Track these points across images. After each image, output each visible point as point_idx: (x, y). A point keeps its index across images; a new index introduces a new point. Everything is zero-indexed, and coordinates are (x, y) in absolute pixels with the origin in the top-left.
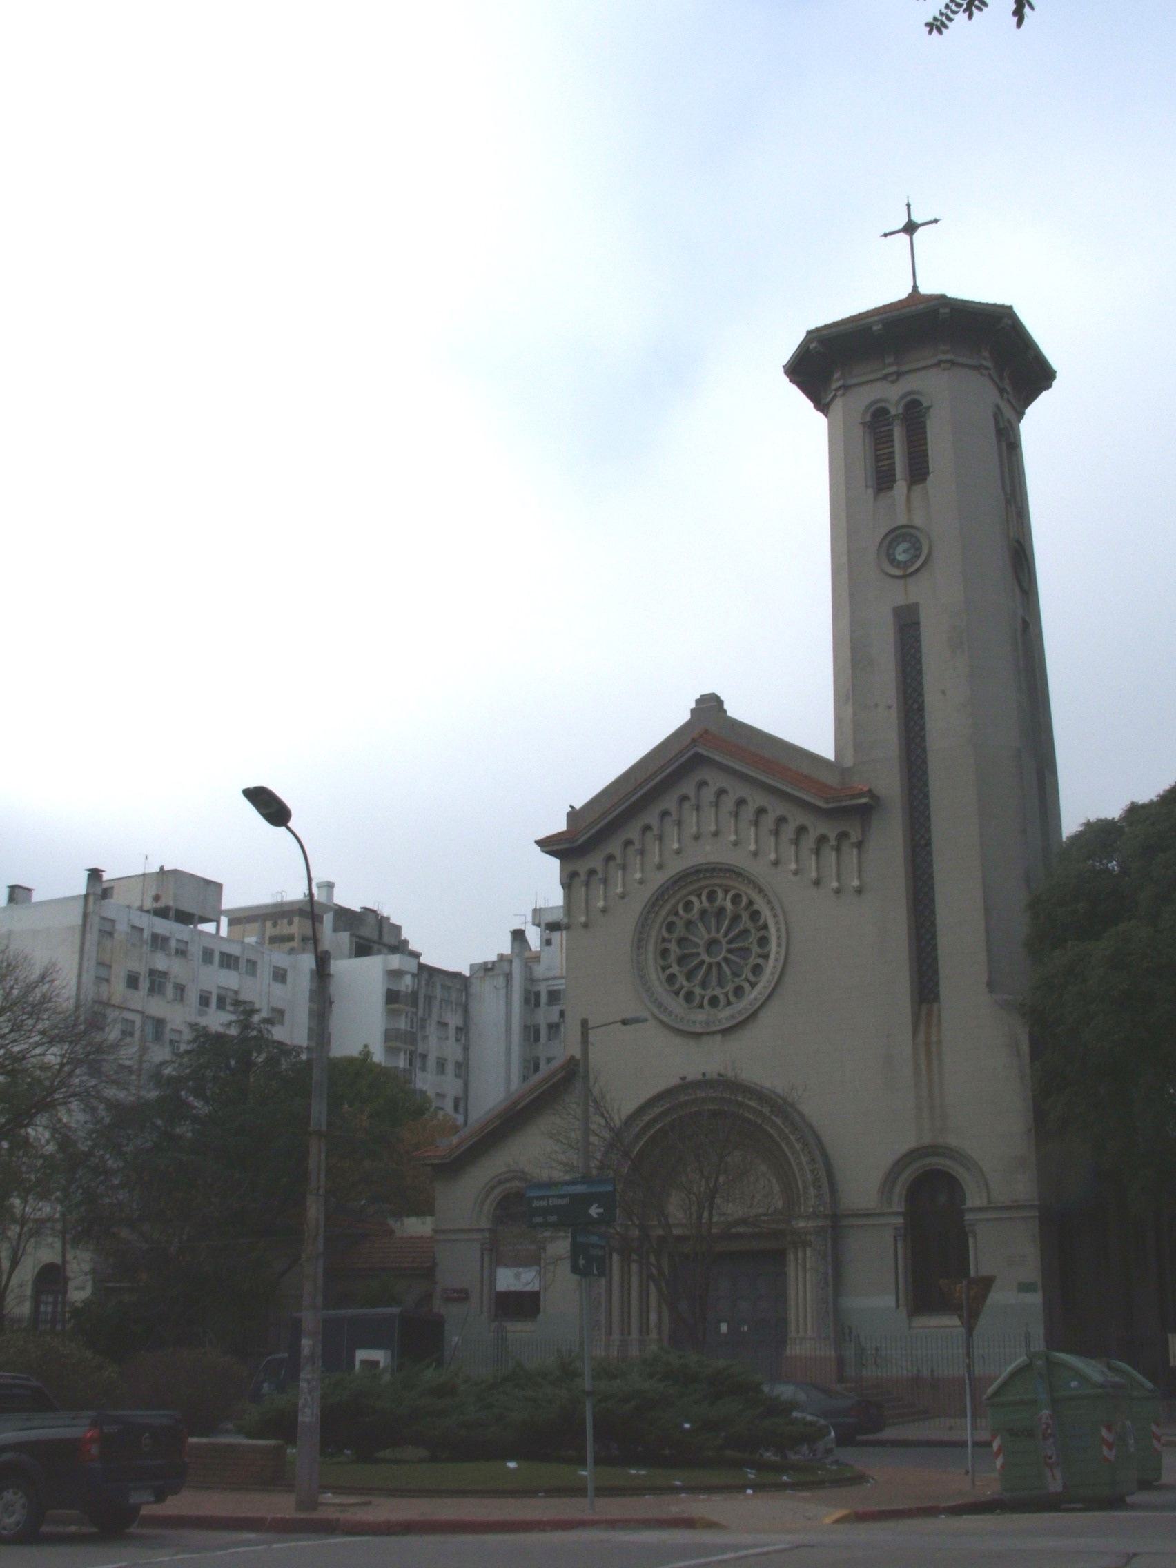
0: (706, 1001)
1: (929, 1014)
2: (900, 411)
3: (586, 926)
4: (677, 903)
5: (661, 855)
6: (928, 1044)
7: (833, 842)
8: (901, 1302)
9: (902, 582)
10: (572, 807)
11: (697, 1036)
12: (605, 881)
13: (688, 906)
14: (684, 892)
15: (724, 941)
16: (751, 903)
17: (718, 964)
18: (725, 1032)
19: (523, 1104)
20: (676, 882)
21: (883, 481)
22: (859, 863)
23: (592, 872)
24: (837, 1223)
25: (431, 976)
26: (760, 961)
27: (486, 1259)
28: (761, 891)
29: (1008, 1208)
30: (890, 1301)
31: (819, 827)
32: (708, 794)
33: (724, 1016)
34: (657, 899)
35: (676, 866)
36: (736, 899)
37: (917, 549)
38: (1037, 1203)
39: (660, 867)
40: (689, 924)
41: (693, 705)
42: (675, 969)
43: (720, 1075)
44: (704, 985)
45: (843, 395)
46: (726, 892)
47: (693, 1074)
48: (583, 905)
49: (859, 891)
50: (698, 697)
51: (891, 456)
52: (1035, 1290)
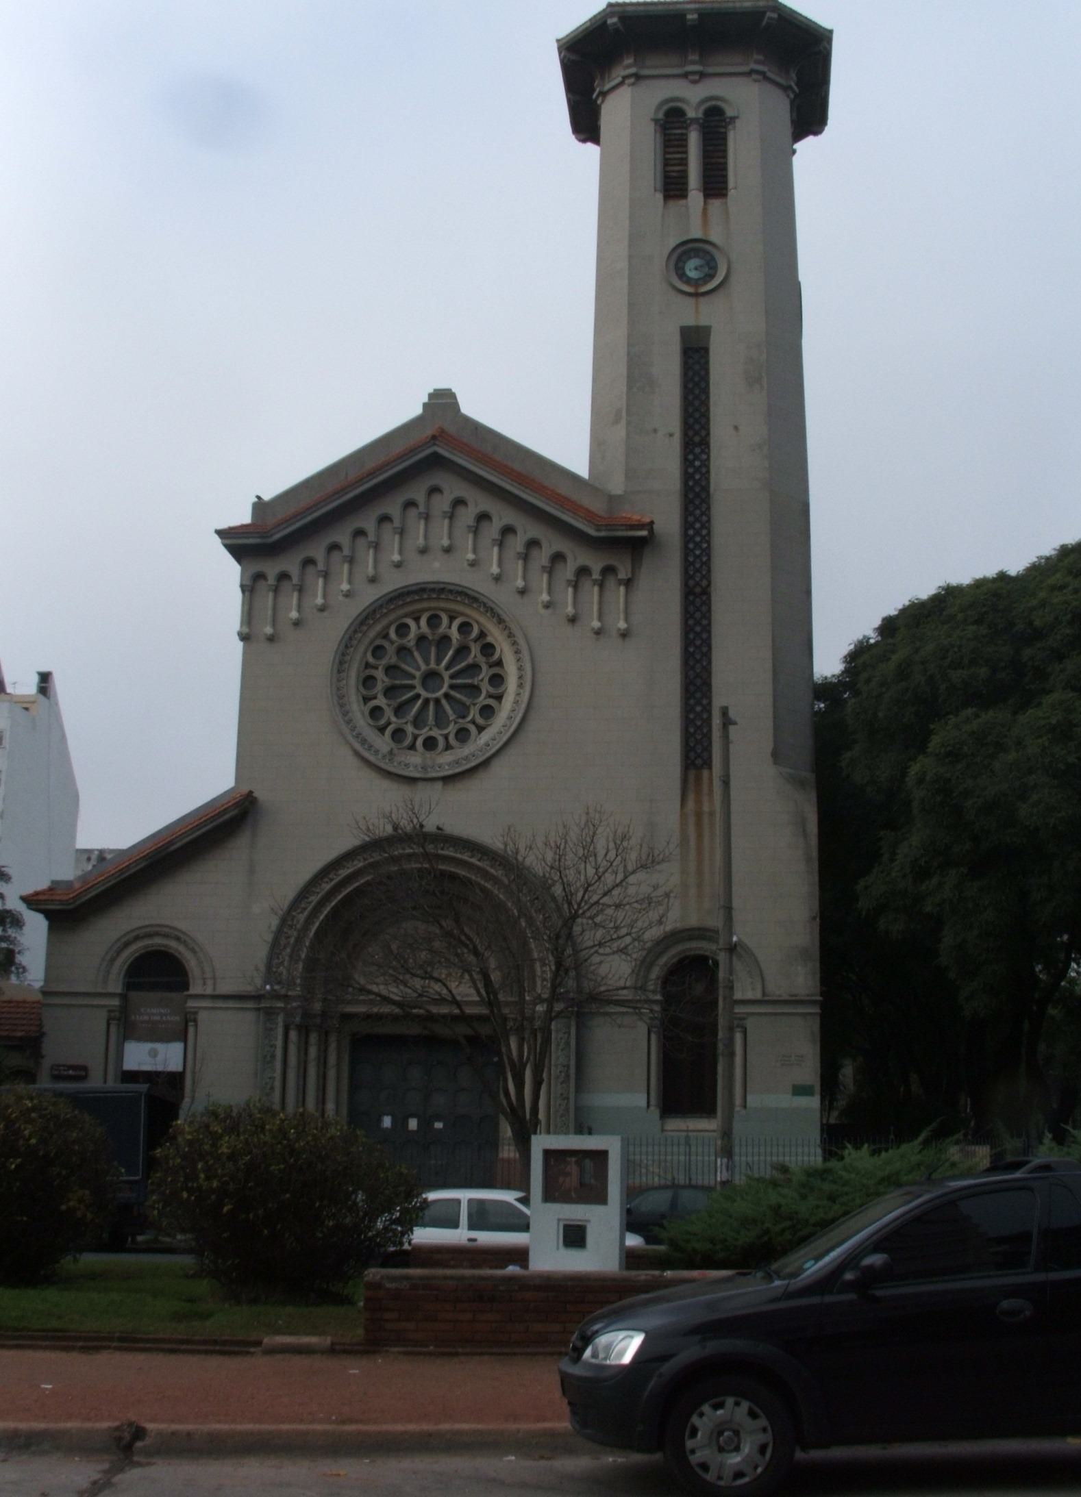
0: (419, 742)
1: (698, 779)
2: (700, 115)
3: (271, 639)
4: (388, 627)
5: (375, 567)
6: (699, 815)
7: (596, 575)
8: (653, 1101)
9: (692, 300)
10: (258, 497)
11: (412, 781)
12: (301, 589)
13: (403, 629)
14: (401, 612)
15: (446, 675)
16: (482, 635)
17: (437, 701)
18: (446, 780)
19: (179, 845)
20: (391, 600)
21: (673, 188)
22: (600, 603)
23: (284, 576)
24: (584, 1005)
26: (491, 702)
27: (113, 1029)
28: (501, 621)
29: (786, 1002)
30: (641, 1100)
31: (577, 557)
32: (442, 503)
33: (445, 761)
34: (367, 618)
35: (393, 582)
36: (465, 628)
37: (710, 268)
38: (819, 998)
39: (373, 580)
40: (402, 650)
41: (426, 399)
42: (381, 701)
43: (438, 828)
44: (418, 722)
45: (633, 84)
46: (452, 619)
48: (270, 612)
49: (624, 635)
50: (431, 391)
51: (684, 162)
52: (812, 1094)
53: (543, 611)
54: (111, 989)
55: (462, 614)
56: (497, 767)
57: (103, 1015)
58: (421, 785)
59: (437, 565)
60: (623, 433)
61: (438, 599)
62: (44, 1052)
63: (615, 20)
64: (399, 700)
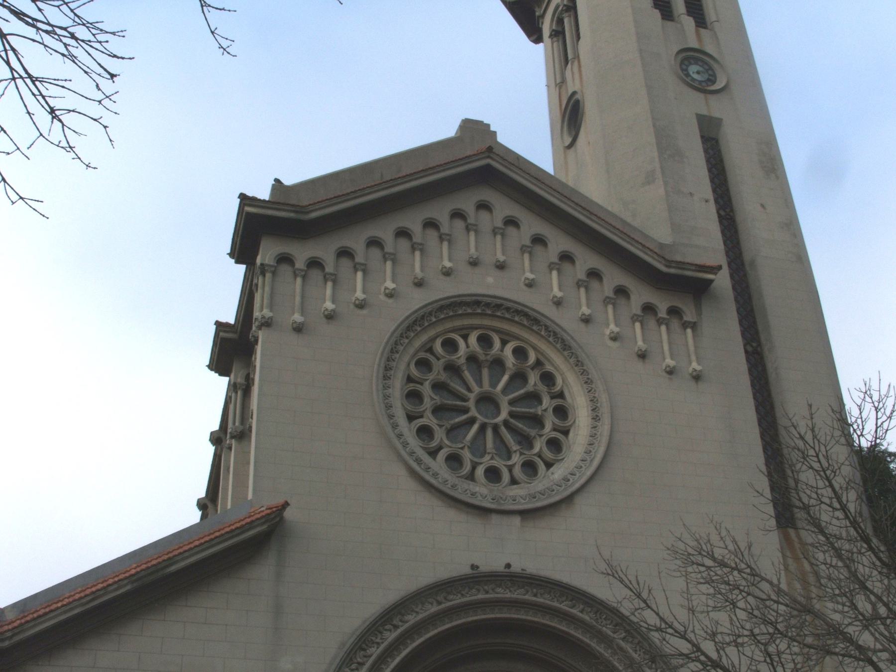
4: (433, 340)
13: (450, 345)
14: (449, 325)
18: (525, 514)
20: (441, 309)
23: (315, 264)
25: (245, 205)
31: (641, 294)
33: (519, 495)
34: (415, 322)
35: (444, 289)
36: (520, 353)
42: (429, 420)
47: (493, 563)
53: (611, 343)
55: (517, 338)
56: (582, 504)
58: (495, 518)
59: (490, 280)
60: (661, 191)
61: (493, 316)
64: (452, 422)
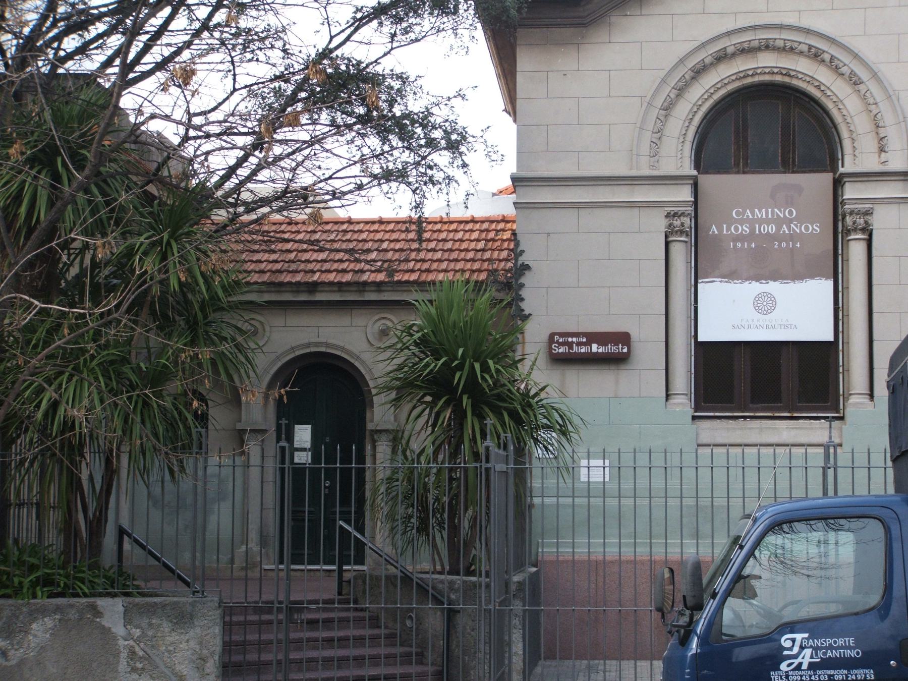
54: (668, 167)
57: (658, 223)
62: (527, 307)
63: (303, 434)
